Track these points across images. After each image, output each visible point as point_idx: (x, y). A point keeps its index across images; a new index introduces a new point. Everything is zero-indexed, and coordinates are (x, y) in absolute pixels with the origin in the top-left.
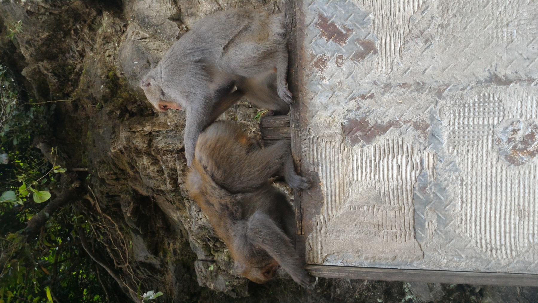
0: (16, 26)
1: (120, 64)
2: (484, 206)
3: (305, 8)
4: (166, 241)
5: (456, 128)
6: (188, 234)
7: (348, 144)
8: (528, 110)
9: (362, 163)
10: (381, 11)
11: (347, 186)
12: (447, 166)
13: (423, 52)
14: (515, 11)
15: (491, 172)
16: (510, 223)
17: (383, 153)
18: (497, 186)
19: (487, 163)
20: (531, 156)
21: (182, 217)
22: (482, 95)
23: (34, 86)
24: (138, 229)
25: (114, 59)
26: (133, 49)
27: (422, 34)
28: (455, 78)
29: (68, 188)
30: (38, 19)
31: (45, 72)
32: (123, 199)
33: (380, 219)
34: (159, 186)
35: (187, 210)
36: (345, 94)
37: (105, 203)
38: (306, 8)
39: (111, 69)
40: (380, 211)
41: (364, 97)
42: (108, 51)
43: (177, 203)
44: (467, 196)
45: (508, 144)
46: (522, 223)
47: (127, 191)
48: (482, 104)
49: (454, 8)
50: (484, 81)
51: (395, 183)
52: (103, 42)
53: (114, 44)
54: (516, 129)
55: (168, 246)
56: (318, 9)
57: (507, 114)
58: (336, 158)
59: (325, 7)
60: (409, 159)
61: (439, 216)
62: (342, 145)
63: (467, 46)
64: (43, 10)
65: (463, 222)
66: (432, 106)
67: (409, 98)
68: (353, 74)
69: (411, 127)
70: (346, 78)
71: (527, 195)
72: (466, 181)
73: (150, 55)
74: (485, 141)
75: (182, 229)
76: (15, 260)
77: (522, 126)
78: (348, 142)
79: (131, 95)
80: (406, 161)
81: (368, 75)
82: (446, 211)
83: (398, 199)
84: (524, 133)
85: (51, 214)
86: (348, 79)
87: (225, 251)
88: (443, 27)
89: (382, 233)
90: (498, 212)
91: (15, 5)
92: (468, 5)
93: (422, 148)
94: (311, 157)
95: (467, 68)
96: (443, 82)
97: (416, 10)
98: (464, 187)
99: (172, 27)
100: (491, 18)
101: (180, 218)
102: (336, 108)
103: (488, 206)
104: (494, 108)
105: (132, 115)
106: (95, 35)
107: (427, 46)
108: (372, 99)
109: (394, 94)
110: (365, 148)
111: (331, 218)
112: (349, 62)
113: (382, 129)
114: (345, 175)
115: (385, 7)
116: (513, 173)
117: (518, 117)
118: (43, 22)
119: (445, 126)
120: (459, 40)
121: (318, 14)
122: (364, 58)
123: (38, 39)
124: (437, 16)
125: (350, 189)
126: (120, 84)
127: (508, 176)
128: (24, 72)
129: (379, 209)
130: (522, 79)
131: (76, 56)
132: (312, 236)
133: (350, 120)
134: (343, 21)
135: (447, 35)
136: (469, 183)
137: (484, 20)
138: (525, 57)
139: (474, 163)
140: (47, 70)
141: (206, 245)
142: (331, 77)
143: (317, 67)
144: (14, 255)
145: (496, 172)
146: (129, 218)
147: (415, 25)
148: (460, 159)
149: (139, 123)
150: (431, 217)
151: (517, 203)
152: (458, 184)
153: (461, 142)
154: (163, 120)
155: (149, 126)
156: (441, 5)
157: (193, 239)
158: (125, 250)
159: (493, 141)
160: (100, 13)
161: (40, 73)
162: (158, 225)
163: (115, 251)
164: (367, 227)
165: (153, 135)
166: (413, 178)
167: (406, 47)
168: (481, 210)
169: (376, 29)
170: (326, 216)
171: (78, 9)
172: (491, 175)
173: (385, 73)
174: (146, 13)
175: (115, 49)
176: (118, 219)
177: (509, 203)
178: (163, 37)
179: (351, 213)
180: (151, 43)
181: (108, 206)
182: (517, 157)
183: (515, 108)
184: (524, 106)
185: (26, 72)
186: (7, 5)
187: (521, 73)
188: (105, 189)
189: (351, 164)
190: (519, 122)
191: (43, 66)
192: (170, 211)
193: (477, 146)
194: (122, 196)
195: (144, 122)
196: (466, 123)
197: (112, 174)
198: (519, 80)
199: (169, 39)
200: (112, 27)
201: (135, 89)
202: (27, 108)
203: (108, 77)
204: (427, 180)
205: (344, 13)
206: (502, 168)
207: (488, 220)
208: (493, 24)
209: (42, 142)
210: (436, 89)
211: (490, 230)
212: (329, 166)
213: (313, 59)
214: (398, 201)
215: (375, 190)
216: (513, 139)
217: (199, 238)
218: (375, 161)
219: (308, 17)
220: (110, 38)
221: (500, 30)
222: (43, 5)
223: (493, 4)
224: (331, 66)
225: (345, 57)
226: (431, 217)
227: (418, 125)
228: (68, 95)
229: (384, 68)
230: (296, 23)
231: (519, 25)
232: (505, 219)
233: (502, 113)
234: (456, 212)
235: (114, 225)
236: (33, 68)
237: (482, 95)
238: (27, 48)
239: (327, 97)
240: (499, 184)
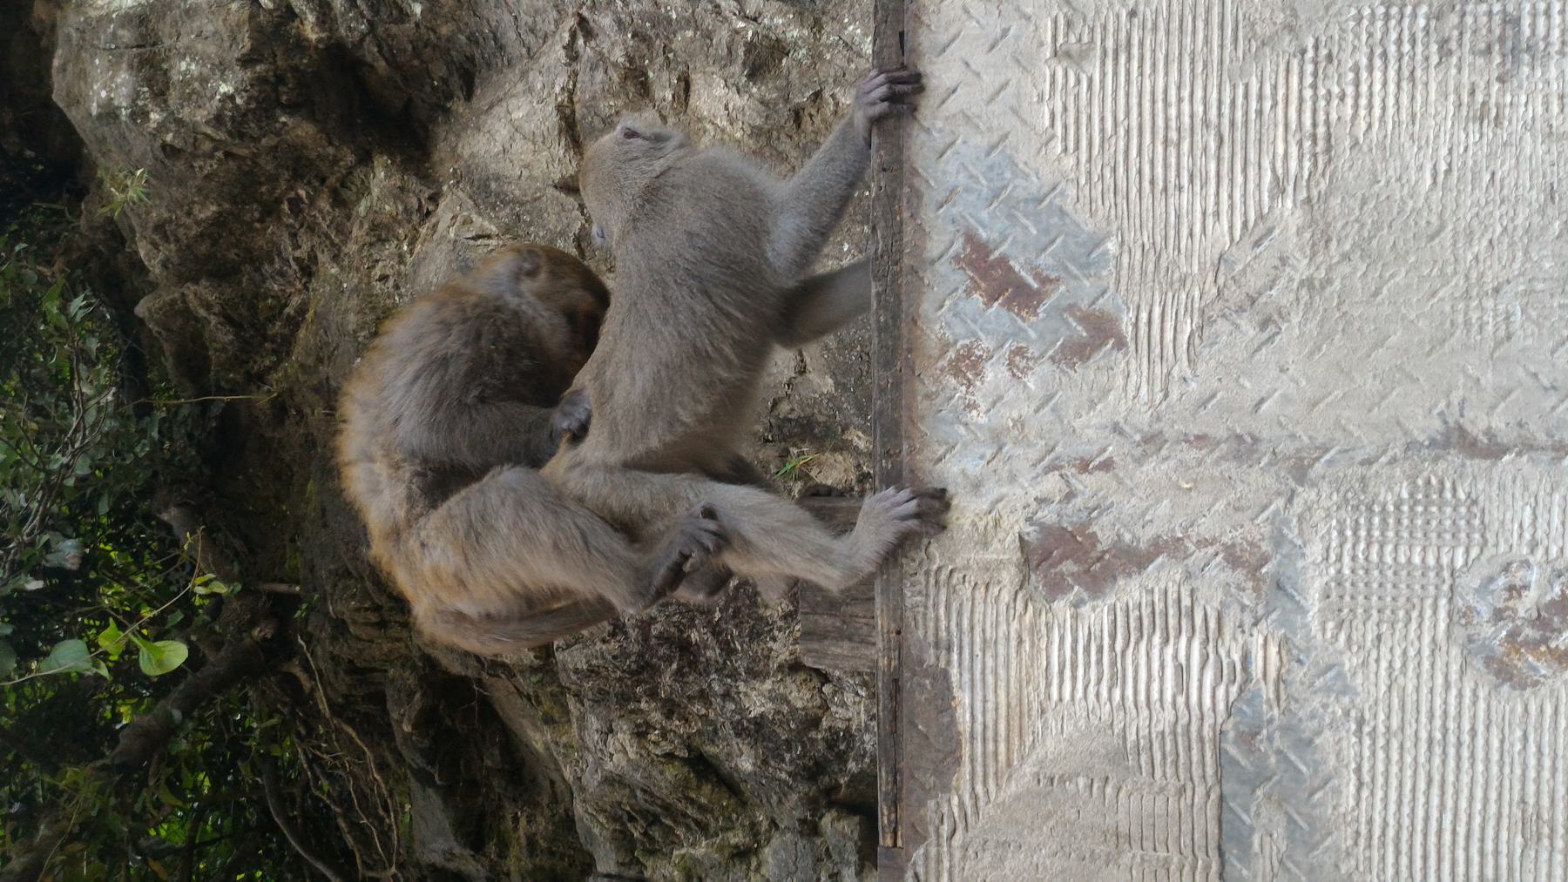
0: (129, 183)
2: (1421, 800)
3: (928, 214)
5: (1347, 571)
6: (572, 794)
7: (1036, 595)
8: (1553, 532)
9: (1074, 650)
10: (1138, 234)
11: (1029, 717)
12: (1318, 676)
13: (1256, 351)
14: (1520, 254)
15: (1445, 702)
16: (1497, 852)
17: (1137, 627)
18: (1459, 744)
19: (1432, 677)
20: (1560, 663)
21: (557, 744)
22: (1420, 482)
23: (168, 348)
24: (432, 771)
25: (397, 287)
27: (1253, 303)
28: (1344, 430)
29: (242, 639)
30: (192, 167)
31: (202, 312)
32: (392, 681)
33: (1121, 815)
35: (575, 726)
36: (1033, 454)
37: (343, 689)
40: (1122, 794)
41: (1084, 466)
42: (380, 264)
43: (547, 704)
44: (1373, 767)
45: (1495, 625)
46: (1532, 854)
47: (407, 658)
48: (1420, 509)
49: (1346, 236)
50: (1427, 443)
51: (1169, 715)
53: (399, 247)
54: (1518, 583)
56: (963, 217)
57: (1491, 541)
58: (1001, 634)
59: (984, 215)
60: (1211, 649)
61: (1291, 820)
62: (1020, 596)
63: (1379, 344)
64: (207, 146)
65: (1362, 842)
66: (1280, 503)
67: (1212, 478)
68: (1054, 401)
69: (1219, 558)
70: (1037, 411)
71: (1546, 774)
72: (1372, 724)
74: (1428, 613)
75: (555, 776)
76: (77, 846)
77: (1534, 576)
78: (1036, 588)
80: (1201, 655)
81: (1099, 407)
82: (1314, 807)
83: (1176, 763)
84: (1540, 596)
85: (187, 714)
86: (1041, 413)
87: (676, 853)
88: (1314, 288)
89: (1126, 859)
90: (1463, 817)
91: (131, 126)
92: (1386, 230)
93: (1248, 620)
94: (931, 625)
95: (1379, 405)
96: (1310, 438)
97: (1237, 238)
98: (1367, 741)
99: (564, 210)
100: (1449, 270)
101: (552, 746)
102: (1004, 490)
103: (1435, 801)
104: (1454, 522)
106: (348, 217)
107: (1265, 335)
108: (1107, 471)
109: (1172, 463)
110: (1085, 610)
111: (981, 803)
112: (1045, 368)
113: (1135, 559)
114: (1024, 683)
115: (1150, 225)
116: (1508, 708)
117: (1525, 550)
118: (207, 177)
119: (1313, 563)
120: (1357, 324)
122: (1089, 358)
123: (189, 221)
124: (1298, 255)
125: (1039, 724)
127: (1494, 719)
128: (141, 309)
129: (1119, 790)
130: (1536, 444)
131: (291, 272)
132: (926, 856)
133: (1044, 528)
134: (1033, 256)
135: (1325, 310)
136: (1381, 729)
137: (1429, 275)
138: (1547, 383)
139: (1397, 673)
140: (208, 307)
141: (621, 831)
142: (994, 404)
143: (956, 376)
144: (77, 830)
145: (1460, 703)
146: (406, 737)
147: (1233, 278)
148: (1355, 660)
150: (1270, 821)
151: (1516, 797)
152: (1348, 731)
153: (1360, 611)
156: (1310, 226)
157: (586, 811)
158: (390, 826)
159: (1450, 615)
160: (365, 159)
161: (187, 313)
162: (488, 763)
163: (361, 828)
164: (1085, 837)
166: (1221, 706)
167: (1206, 334)
168: (1413, 810)
169: (1124, 281)
170: (967, 798)
171: (304, 147)
172: (1445, 712)
173: (1146, 404)
174: (493, 167)
175: (401, 259)
176: (376, 738)
177: (1493, 795)
178: (537, 235)
179: (1039, 794)
181: (352, 699)
182: (1519, 665)
183: (1516, 526)
184: (1540, 520)
185: (149, 310)
186: (108, 124)
187: (1532, 427)
188: (343, 650)
189: (1044, 653)
190: (1526, 564)
191: (196, 294)
192: (525, 722)
193: (1406, 626)
194: (391, 672)
196: (1374, 557)
197: (366, 610)
198: (1528, 446)
200: (396, 198)
202: (144, 411)
204: (1259, 714)
205: (1035, 232)
206: (1475, 693)
207: (1432, 839)
208: (1457, 285)
209: (178, 506)
210: (1290, 458)
211: (1439, 869)
212: (980, 654)
213: (944, 353)
214: (1177, 768)
215: (1110, 732)
216: (1509, 613)
217: (603, 811)
218: (1112, 647)
219: (936, 237)
220: (389, 228)
221: (1475, 303)
222: (209, 131)
223: (1456, 233)
224: (995, 373)
225: (1033, 351)
226: (1270, 821)
227: (1239, 553)
228: (260, 378)
229: (1144, 390)
230: (901, 252)
231: (1527, 293)
232: (1482, 840)
233: (1477, 536)
234: (1342, 810)
235: (364, 753)
236: (167, 299)
237: (1420, 482)
238: (155, 245)
239: (982, 457)
240: (1466, 738)
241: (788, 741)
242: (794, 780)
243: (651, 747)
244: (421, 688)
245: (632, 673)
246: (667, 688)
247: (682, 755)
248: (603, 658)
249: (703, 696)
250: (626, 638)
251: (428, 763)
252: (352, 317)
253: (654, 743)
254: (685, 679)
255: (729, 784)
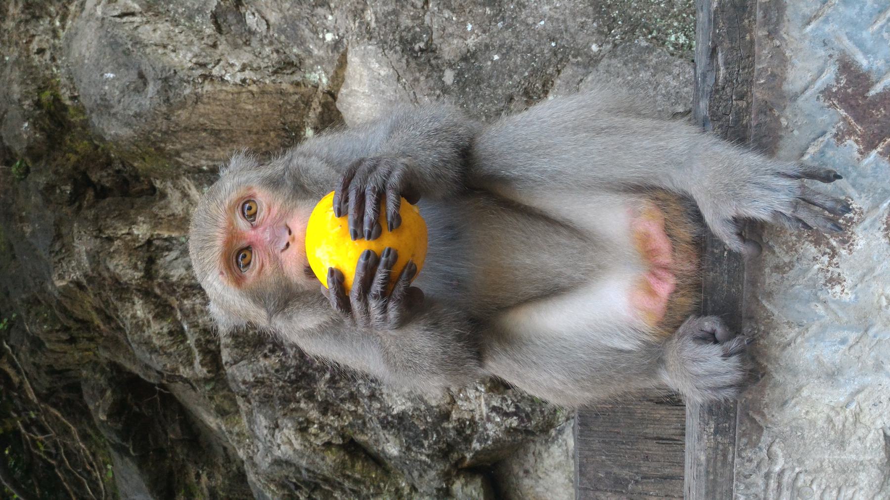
1: (69, 72)
4: (192, 471)
21: (231, 433)
24: (127, 446)
25: (53, 59)
26: (99, 42)
32: (86, 380)
34: (177, 369)
38: (795, 34)
39: (47, 84)
42: (37, 38)
52: (23, 16)
53: (52, 23)
55: (194, 480)
73: (145, 60)
79: (97, 147)
102: (869, 379)
105: (102, 193)
121: (836, 57)
126: (70, 122)
141: (288, 495)
149: (120, 215)
154: (180, 208)
155: (144, 222)
157: (259, 480)
162: (172, 436)
165: (157, 248)
175: (55, 34)
176: (77, 416)
178: (176, 12)
180: (148, 27)
188: (43, 360)
192: (200, 409)
195: (132, 212)
197: (58, 331)
199: (190, 18)
201: (108, 138)
203: (38, 104)
217: (273, 480)
219: (799, 64)
230: (749, 82)
235: (70, 428)
239: (843, 341)
241: (425, 431)
242: (432, 460)
243: (312, 439)
244: (111, 386)
245: (292, 382)
246: (322, 393)
247: (337, 442)
248: (267, 371)
249: (353, 398)
250: (285, 354)
251: (123, 440)
252: (16, 88)
253: (314, 435)
254: (337, 385)
255: (377, 461)
